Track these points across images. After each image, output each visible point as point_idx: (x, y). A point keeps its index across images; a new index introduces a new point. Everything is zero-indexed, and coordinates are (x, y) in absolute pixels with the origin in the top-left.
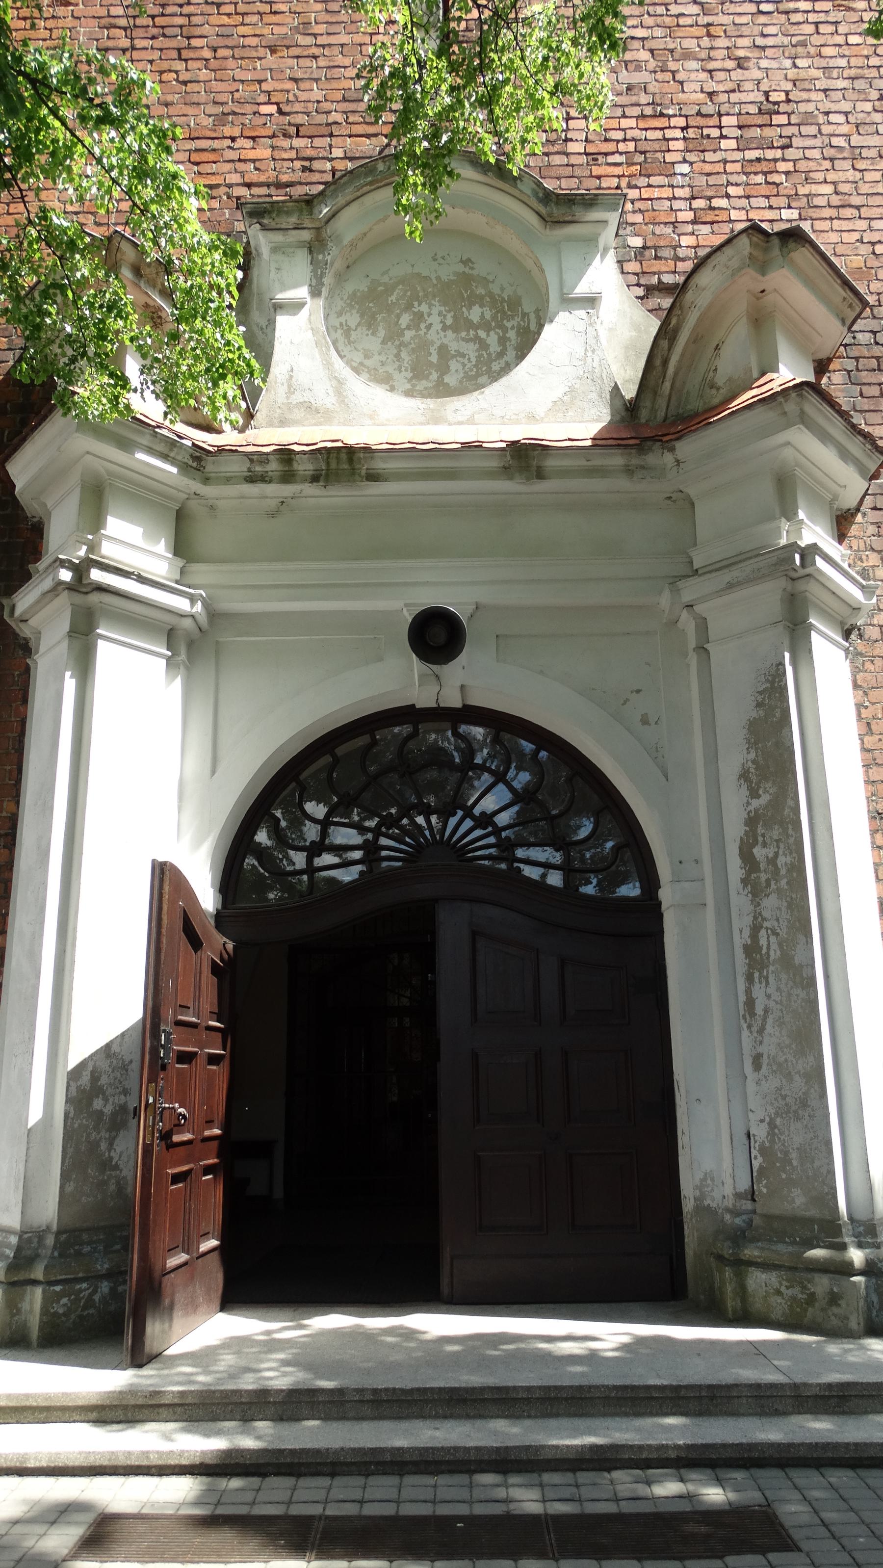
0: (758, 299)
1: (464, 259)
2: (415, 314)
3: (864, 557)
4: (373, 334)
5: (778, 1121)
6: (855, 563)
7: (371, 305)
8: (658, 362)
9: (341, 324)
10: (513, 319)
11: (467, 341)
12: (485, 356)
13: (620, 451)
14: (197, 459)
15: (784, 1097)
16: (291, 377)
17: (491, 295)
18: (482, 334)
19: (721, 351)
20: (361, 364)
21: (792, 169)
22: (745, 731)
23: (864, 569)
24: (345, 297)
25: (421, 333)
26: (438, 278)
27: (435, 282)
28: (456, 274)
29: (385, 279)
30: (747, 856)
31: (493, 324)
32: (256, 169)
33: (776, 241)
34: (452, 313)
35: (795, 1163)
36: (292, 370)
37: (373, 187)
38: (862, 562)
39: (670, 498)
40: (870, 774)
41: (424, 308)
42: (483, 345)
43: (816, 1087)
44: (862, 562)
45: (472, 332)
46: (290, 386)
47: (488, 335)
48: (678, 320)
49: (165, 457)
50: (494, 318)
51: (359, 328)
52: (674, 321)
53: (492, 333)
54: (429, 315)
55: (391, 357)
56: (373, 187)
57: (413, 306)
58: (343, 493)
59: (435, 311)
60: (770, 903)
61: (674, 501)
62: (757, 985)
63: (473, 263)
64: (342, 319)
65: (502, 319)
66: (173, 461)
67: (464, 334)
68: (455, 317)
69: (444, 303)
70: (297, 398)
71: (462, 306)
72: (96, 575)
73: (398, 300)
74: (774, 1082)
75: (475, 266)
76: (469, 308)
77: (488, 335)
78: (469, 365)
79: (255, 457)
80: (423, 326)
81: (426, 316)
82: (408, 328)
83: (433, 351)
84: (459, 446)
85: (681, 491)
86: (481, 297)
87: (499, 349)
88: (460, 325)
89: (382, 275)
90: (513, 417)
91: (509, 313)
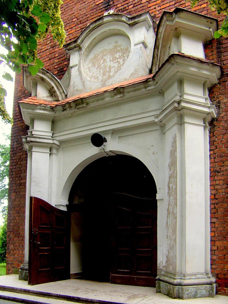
0: (176, 31)
1: (115, 42)
2: (104, 60)
3: (219, 97)
4: (95, 67)
5: (169, 250)
6: (216, 99)
7: (94, 60)
8: (156, 56)
9: (88, 67)
10: (126, 54)
11: (115, 63)
12: (119, 65)
13: (142, 84)
14: (52, 109)
15: (170, 245)
16: (74, 84)
17: (121, 49)
18: (119, 60)
19: (171, 48)
20: (92, 76)
21: (128, 9)
22: (170, 154)
23: (219, 101)
24: (89, 60)
25: (105, 64)
26: (109, 49)
27: (109, 50)
28: (114, 46)
29: (98, 53)
30: (169, 187)
31: (122, 56)
32: (72, 35)
33: (174, 14)
34: (112, 57)
35: (171, 260)
36: (74, 82)
37: (90, 32)
38: (219, 99)
39: (160, 92)
40: (215, 160)
41: (106, 57)
42: (119, 62)
43: (175, 242)
44: (219, 99)
45: (117, 60)
46: (74, 86)
47: (120, 60)
48: (158, 43)
49: (44, 110)
50: (122, 55)
51: (92, 67)
52: (157, 44)
53: (121, 59)
54: (107, 59)
55: (98, 72)
56: (90, 32)
57: (103, 58)
58: (83, 109)
59: (108, 57)
60: (172, 198)
61: (161, 93)
62: (168, 218)
63: (117, 42)
64: (88, 66)
65: (124, 54)
66: (47, 110)
67: (115, 61)
68: (113, 58)
69: (110, 55)
70: (76, 88)
71: (114, 54)
72: (183, 104)
73: (100, 57)
74: (169, 242)
75: (118, 43)
76: (116, 54)
77: (120, 60)
78: (116, 69)
79: (63, 106)
80: (105, 62)
81: (106, 59)
82: (102, 64)
83: (108, 68)
84: (103, 92)
85: (162, 90)
86: (119, 50)
87: (122, 63)
88: (114, 59)
89: (97, 52)
90: (121, 80)
91: (125, 52)
